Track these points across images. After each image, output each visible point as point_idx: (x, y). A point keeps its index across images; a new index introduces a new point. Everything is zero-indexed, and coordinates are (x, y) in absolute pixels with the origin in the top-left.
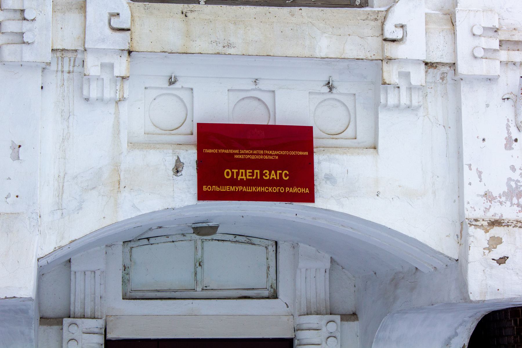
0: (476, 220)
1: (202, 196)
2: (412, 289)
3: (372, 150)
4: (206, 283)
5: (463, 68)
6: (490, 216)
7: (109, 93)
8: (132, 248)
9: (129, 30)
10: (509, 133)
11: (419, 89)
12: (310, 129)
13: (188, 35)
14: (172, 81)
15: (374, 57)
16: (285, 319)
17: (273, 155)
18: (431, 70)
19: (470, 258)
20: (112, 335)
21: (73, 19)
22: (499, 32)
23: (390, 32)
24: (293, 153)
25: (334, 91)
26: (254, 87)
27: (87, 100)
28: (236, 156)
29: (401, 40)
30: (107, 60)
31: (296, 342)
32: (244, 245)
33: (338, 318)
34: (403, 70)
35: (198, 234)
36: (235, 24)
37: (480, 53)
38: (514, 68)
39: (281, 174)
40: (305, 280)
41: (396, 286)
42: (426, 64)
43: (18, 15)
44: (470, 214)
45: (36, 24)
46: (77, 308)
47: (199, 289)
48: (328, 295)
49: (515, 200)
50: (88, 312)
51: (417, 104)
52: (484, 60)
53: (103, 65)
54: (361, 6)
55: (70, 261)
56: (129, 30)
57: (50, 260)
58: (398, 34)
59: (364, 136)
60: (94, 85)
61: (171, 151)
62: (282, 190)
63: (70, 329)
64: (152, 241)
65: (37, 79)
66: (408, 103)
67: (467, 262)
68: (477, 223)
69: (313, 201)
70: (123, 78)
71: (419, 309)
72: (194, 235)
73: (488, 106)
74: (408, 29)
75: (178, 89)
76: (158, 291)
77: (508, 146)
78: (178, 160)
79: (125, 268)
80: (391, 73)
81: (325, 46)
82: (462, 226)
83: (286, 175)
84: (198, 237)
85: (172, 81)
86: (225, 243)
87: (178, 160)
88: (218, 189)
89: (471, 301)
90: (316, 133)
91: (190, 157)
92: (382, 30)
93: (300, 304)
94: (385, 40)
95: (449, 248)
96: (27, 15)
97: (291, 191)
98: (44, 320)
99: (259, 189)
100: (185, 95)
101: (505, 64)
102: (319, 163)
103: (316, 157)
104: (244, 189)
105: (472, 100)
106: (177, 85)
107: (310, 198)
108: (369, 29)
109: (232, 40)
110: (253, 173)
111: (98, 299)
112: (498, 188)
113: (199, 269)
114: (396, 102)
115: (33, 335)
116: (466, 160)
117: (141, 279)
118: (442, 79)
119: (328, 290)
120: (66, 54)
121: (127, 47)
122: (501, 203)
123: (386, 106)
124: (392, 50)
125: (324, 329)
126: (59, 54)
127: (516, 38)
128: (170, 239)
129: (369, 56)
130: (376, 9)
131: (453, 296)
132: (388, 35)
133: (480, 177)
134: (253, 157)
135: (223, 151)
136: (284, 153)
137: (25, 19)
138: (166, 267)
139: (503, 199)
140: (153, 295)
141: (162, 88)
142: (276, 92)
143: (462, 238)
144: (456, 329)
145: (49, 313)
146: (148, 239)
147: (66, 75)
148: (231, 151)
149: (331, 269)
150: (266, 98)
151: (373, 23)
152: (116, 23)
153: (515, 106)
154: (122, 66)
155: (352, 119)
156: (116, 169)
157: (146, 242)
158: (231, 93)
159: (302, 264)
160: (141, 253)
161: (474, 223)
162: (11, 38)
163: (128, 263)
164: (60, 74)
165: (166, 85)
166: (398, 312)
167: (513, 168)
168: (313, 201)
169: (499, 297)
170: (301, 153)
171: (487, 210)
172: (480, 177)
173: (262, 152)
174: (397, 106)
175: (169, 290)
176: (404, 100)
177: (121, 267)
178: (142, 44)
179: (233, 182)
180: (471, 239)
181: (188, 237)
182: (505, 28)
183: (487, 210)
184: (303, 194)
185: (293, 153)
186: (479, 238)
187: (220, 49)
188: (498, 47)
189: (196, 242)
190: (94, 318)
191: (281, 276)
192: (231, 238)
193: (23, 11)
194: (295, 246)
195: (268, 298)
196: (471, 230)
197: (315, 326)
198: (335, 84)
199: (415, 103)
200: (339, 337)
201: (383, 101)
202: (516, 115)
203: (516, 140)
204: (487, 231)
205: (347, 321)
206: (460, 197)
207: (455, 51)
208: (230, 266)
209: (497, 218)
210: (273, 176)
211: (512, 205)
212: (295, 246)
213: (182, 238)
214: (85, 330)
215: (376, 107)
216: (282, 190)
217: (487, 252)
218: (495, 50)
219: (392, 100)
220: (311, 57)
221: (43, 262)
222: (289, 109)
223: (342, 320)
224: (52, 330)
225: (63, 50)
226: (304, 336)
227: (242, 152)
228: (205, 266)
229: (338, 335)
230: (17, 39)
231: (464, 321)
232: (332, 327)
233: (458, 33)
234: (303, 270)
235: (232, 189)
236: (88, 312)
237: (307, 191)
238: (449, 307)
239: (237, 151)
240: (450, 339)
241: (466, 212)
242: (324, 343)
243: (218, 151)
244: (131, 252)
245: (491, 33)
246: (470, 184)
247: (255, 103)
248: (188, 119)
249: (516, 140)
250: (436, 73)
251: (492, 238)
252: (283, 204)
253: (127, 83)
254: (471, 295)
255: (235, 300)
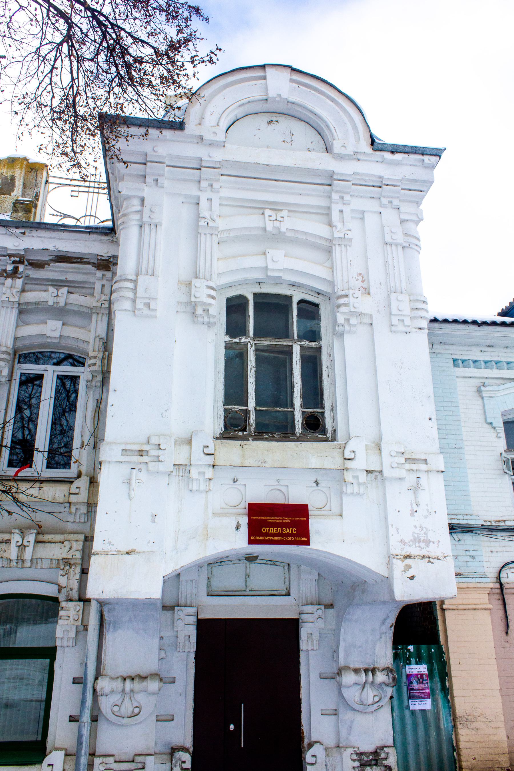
0: (397, 555)
1: (251, 542)
2: (364, 592)
3: (340, 517)
4: (252, 587)
5: (386, 473)
6: (404, 553)
7: (203, 487)
8: (212, 567)
9: (213, 454)
10: (412, 508)
11: (363, 484)
12: (307, 506)
13: (243, 457)
14: (235, 481)
15: (339, 468)
16: (294, 607)
17: (288, 520)
18: (369, 474)
19: (395, 577)
20: (201, 616)
21: (185, 448)
22: (405, 454)
23: (347, 455)
24: (298, 519)
25: (319, 485)
26: (277, 483)
27: (191, 491)
28: (269, 521)
29: (353, 459)
30: (202, 470)
31: (300, 621)
32: (271, 566)
33: (323, 607)
34: (355, 475)
35: (248, 560)
36: (267, 451)
37: (395, 465)
38: (413, 473)
39: (292, 530)
40: (305, 586)
41: (354, 590)
42: (367, 471)
43: (157, 447)
44: (394, 552)
45: (166, 451)
46: (182, 601)
47: (248, 590)
48: (317, 593)
49: (417, 544)
50: (188, 604)
51: (363, 493)
52: (397, 469)
53: (199, 473)
54: (332, 441)
55: (179, 574)
56: (213, 454)
57: (169, 576)
58: (352, 456)
59: (335, 510)
60: (195, 483)
61: (234, 518)
62: (293, 539)
63: (179, 613)
64: (223, 563)
65: (166, 480)
66: (358, 492)
67: (393, 579)
68: (398, 557)
69: (309, 545)
70: (210, 479)
71: (367, 604)
72: (245, 561)
73: (400, 493)
74: (357, 453)
75: (238, 485)
76: (226, 591)
77: (412, 515)
78: (238, 523)
79: (208, 578)
80: (349, 476)
81: (314, 462)
82: (390, 558)
83: (295, 531)
84: (247, 562)
85: (235, 481)
86: (262, 565)
87: (238, 523)
88: (259, 538)
89: (396, 601)
90: (310, 508)
91: (244, 521)
92: (343, 454)
93: (302, 599)
94: (345, 459)
95: (383, 571)
96: (161, 447)
97: (297, 539)
98: (165, 608)
99: (281, 538)
100: (242, 488)
101: (408, 471)
102: (312, 524)
103: (310, 521)
104: (273, 538)
105: (391, 489)
106: (238, 483)
107: (307, 543)
108: (337, 453)
109: (266, 459)
110: (277, 530)
111: (193, 596)
112: (408, 538)
113: (248, 579)
114: (352, 491)
115: (159, 617)
116: (390, 522)
117: (218, 585)
118: (375, 479)
119: (317, 591)
120: (182, 467)
121: (212, 464)
122: (410, 546)
123: (346, 493)
124: (348, 464)
125: (315, 613)
126: (177, 467)
127: (413, 457)
128: (233, 562)
129: (337, 467)
130: (340, 443)
131: (387, 598)
132: (346, 456)
133: (398, 531)
134: (277, 521)
135: (261, 518)
136: (293, 519)
137: (160, 449)
138: (231, 578)
139: (411, 543)
140: (223, 593)
141: (229, 484)
142: (289, 487)
143: (389, 565)
144: (388, 614)
145: (168, 604)
146: (221, 562)
147: (180, 477)
148: (266, 518)
149: (318, 579)
150: (284, 489)
151: (338, 450)
152: (207, 451)
153: (414, 493)
154: (209, 473)
155: (329, 500)
156: (206, 528)
157: (219, 564)
158: (265, 487)
159: (302, 577)
160: (217, 570)
161: (396, 557)
162: (153, 458)
163: (210, 576)
164: (177, 477)
165: (232, 482)
166: (356, 605)
167: (415, 527)
168: (309, 545)
169: (411, 598)
170: (302, 519)
171: (402, 549)
172: (398, 531)
173: (282, 518)
174: (352, 494)
175: (232, 591)
176: (356, 490)
177: (206, 578)
178: (220, 462)
179: (267, 534)
180: (395, 566)
181: (242, 561)
182: (407, 452)
183: (402, 549)
184: (304, 541)
185: (298, 519)
186: (399, 565)
187: (259, 464)
188: (404, 462)
189: (246, 564)
190: (191, 607)
191: (291, 583)
192: (265, 562)
193: (159, 445)
194: (299, 567)
195: (285, 595)
196: (394, 561)
197: (310, 612)
198: (319, 482)
199: (361, 492)
200: (324, 618)
201: (344, 491)
202: (415, 498)
203: (416, 511)
204: (403, 561)
205: (328, 608)
206: (388, 542)
207: (382, 464)
208: (265, 577)
209: (408, 554)
210: (288, 531)
211: (416, 546)
212: (299, 567)
213: (238, 562)
214: (186, 614)
215: (341, 494)
216: (293, 539)
217: (404, 573)
218: (403, 464)
219: (349, 491)
220: (307, 468)
221: (166, 578)
222: (295, 497)
223: (325, 608)
224: (169, 614)
225: (179, 465)
226: (305, 617)
227: (271, 518)
228: (251, 578)
229: (323, 617)
230: (156, 459)
231: (393, 610)
232: (320, 612)
233: (383, 455)
234: (304, 580)
235: (267, 538)
236: (188, 604)
237: (306, 539)
238: (384, 603)
239: (269, 518)
240: (385, 620)
241: (391, 551)
242: (316, 621)
243: (243, 434)
244: (211, 569)
245: (400, 455)
246: (393, 535)
247: (278, 492)
248: (243, 501)
249: (416, 511)
250: (372, 476)
251: (406, 565)
252: (293, 546)
253: (212, 482)
254: (396, 598)
255: (267, 597)
